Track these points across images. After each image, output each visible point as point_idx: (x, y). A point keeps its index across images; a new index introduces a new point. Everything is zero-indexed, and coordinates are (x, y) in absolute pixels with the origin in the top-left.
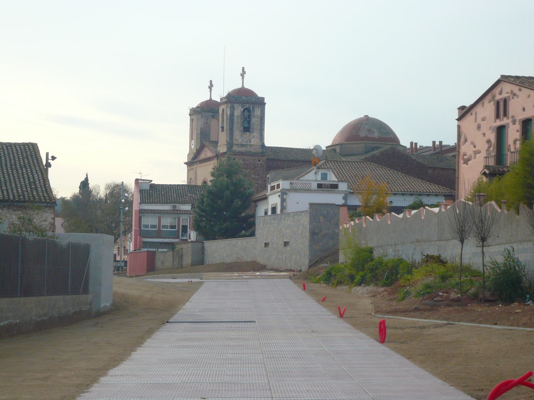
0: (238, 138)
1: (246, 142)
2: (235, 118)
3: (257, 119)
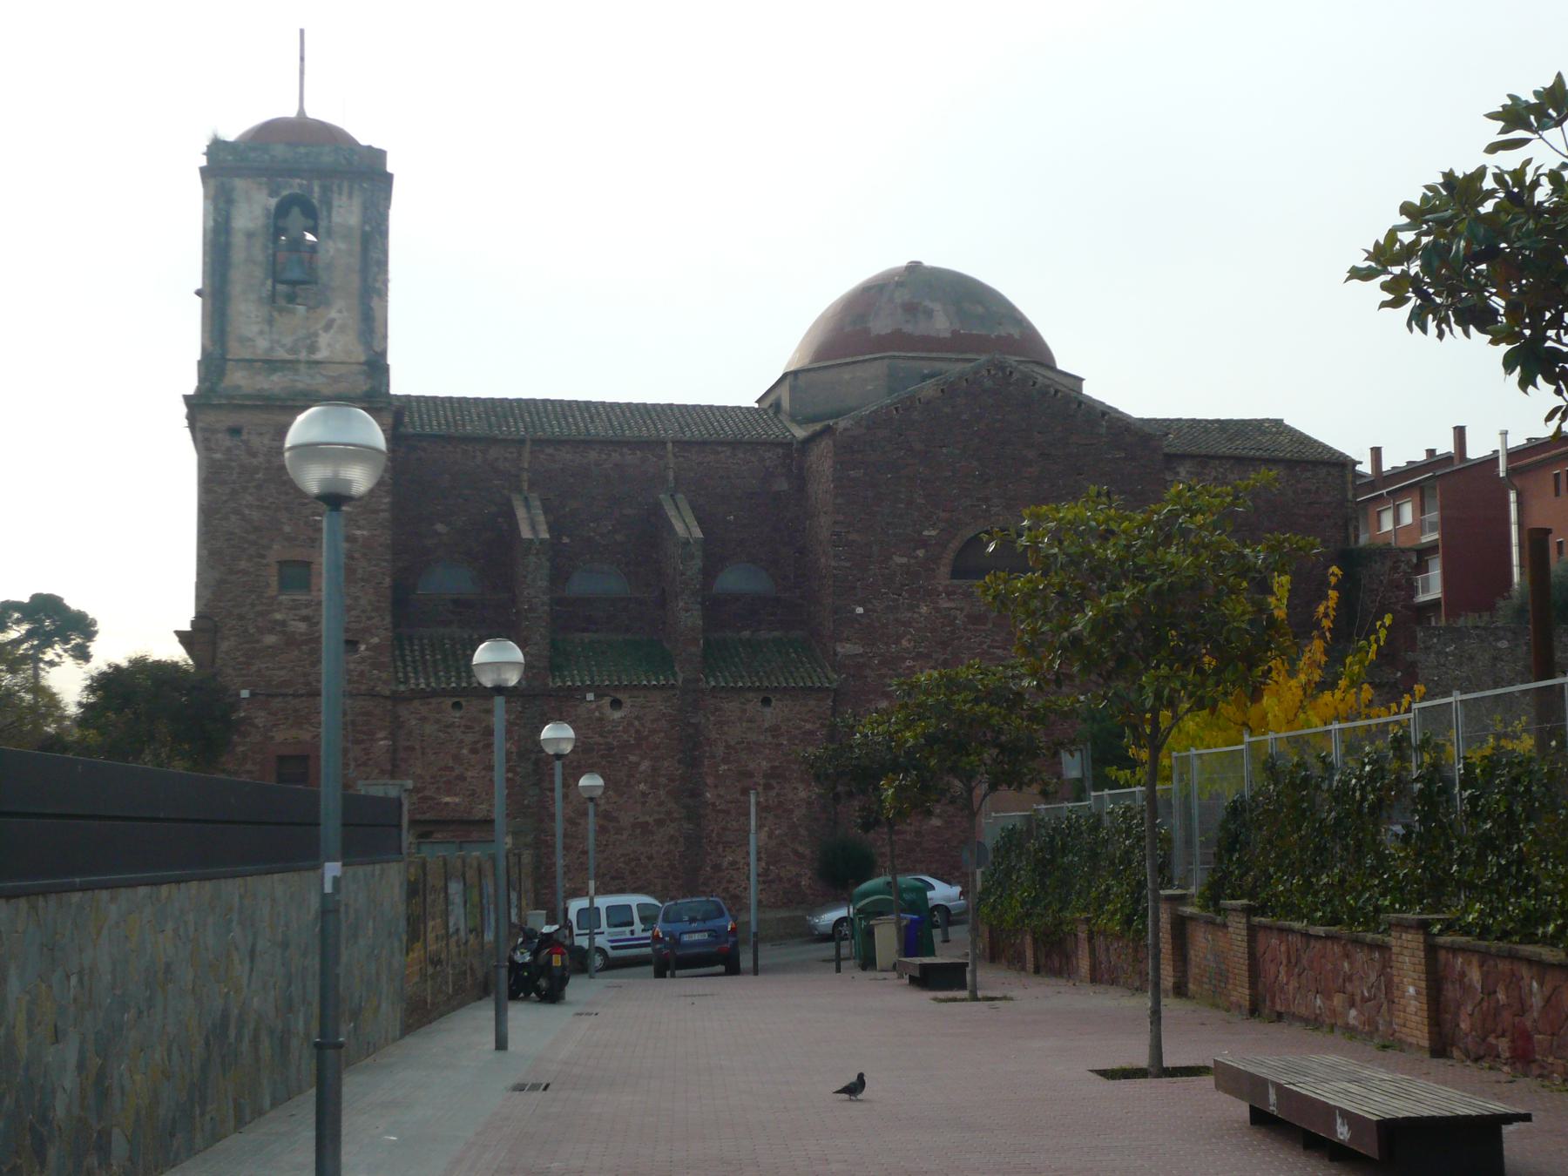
0: (251, 330)
1: (293, 350)
2: (238, 240)
3: (342, 246)
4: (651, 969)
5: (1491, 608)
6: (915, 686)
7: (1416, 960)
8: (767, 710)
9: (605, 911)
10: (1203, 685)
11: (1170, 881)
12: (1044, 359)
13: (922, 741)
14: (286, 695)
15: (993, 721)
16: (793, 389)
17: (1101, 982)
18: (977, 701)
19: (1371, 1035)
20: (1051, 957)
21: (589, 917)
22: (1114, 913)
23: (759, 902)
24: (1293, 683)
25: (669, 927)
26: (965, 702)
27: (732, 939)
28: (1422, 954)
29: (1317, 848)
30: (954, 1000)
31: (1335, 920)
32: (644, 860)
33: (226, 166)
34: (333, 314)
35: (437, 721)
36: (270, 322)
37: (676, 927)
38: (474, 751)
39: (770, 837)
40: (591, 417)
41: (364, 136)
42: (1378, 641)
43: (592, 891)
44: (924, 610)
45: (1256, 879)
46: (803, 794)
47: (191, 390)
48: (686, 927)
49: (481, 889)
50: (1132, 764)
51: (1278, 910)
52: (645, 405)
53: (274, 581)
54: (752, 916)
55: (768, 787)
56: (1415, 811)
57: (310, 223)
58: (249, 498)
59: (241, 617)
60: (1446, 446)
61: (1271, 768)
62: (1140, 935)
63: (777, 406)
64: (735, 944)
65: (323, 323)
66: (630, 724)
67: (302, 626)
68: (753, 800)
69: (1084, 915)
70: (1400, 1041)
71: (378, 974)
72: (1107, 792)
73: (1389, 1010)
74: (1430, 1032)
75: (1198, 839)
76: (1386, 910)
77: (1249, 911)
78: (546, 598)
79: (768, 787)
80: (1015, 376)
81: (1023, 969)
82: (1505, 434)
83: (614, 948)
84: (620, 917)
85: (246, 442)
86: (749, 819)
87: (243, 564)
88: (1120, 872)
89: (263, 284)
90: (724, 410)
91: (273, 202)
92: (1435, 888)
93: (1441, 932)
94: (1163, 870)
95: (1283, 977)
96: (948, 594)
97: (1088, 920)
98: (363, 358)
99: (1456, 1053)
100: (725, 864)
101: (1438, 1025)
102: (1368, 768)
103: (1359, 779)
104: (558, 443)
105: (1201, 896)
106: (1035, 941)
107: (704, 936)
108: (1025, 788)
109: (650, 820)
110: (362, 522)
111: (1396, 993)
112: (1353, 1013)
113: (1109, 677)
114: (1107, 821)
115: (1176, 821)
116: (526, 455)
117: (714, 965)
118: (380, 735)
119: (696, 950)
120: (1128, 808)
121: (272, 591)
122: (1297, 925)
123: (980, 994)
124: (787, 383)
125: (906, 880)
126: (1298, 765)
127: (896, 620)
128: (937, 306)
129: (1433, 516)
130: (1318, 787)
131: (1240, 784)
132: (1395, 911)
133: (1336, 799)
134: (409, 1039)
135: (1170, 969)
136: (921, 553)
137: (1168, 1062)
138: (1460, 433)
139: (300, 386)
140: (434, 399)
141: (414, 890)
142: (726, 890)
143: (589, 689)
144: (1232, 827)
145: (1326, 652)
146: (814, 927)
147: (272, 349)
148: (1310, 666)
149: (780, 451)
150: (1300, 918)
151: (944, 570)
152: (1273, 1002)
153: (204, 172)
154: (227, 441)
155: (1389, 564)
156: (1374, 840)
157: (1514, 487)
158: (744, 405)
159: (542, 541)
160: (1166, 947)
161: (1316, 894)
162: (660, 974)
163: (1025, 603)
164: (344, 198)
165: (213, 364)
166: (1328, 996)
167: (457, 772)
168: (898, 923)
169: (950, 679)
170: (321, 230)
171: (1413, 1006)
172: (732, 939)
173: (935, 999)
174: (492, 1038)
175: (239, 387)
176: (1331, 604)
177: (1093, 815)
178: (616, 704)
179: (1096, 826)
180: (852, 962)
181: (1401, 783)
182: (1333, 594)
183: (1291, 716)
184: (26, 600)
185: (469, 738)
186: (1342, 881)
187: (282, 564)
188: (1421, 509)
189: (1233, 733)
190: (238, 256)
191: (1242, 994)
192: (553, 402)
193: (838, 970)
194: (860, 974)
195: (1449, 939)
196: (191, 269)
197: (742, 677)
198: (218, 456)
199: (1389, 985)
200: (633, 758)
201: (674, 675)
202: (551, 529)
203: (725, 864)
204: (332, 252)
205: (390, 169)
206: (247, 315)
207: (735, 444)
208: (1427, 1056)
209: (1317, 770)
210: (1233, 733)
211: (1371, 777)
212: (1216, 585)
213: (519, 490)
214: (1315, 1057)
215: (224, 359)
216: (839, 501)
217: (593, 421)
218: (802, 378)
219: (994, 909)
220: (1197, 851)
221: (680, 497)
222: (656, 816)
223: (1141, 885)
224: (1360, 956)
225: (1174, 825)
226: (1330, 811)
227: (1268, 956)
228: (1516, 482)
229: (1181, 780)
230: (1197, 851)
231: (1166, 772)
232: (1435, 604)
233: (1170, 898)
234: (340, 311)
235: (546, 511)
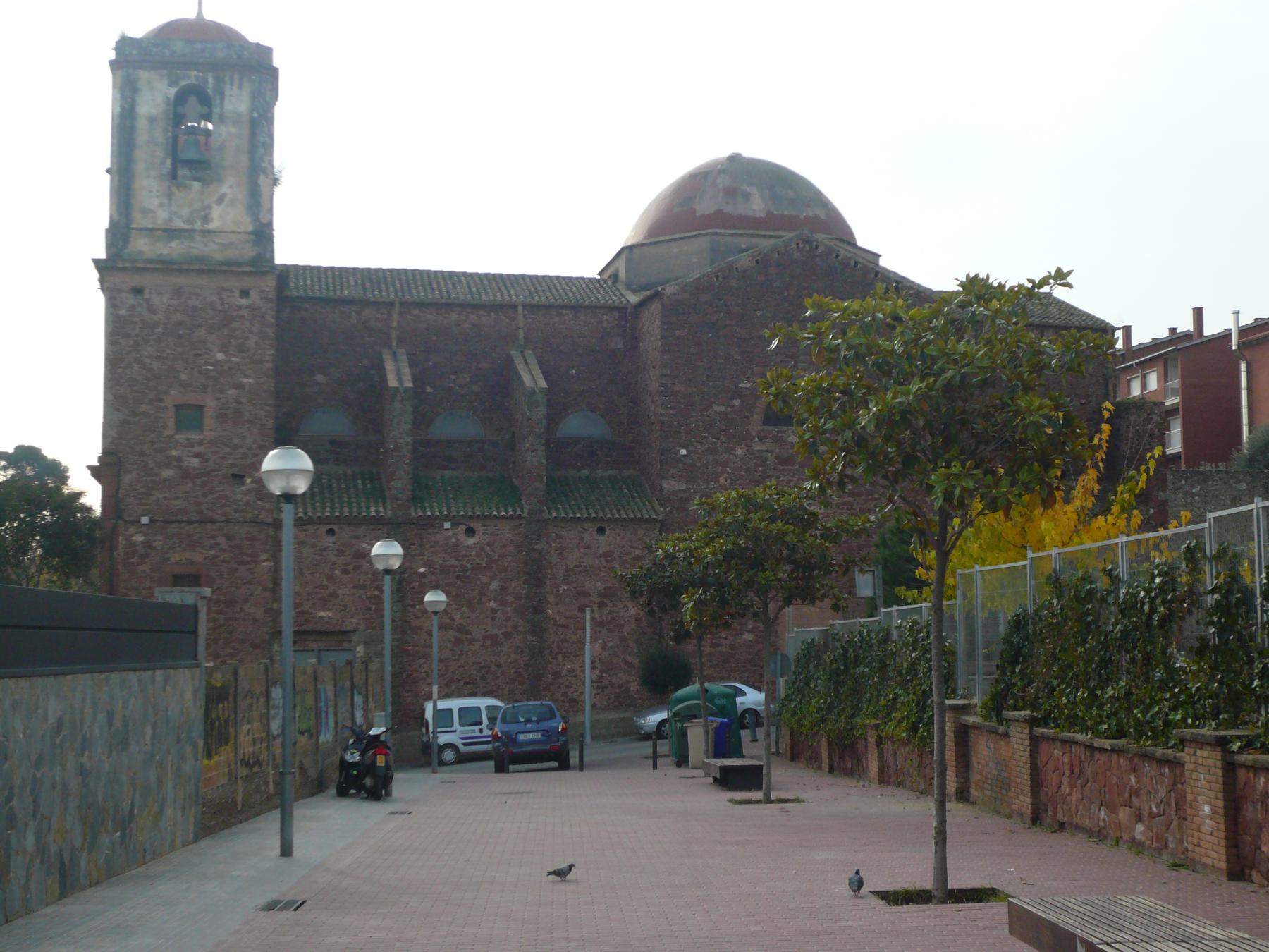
1: (189, 221)
2: (142, 124)
3: (233, 130)
4: (492, 763)
5: (1226, 458)
6: (714, 508)
7: (1213, 778)
8: (602, 539)
9: (456, 714)
10: (997, 485)
11: (954, 691)
12: (846, 237)
13: (720, 557)
14: (180, 522)
15: (788, 539)
16: (628, 261)
17: (888, 783)
18: (773, 520)
19: (1159, 851)
20: (844, 758)
21: (444, 717)
22: (901, 720)
23: (594, 706)
24: (1069, 508)
25: (507, 728)
26: (761, 520)
27: (562, 738)
28: (1220, 772)
29: (1101, 660)
30: (749, 802)
31: (1121, 734)
32: (493, 668)
33: (132, 59)
34: (225, 189)
35: (313, 546)
36: (170, 196)
37: (513, 728)
38: (345, 572)
39: (603, 648)
40: (454, 285)
41: (253, 34)
42: (1147, 471)
43: (435, 696)
44: (739, 452)
45: (1038, 689)
46: (632, 612)
47: (102, 254)
48: (521, 727)
49: (317, 692)
50: (920, 584)
51: (1061, 722)
52: (501, 275)
53: (171, 422)
54: (587, 717)
55: (602, 605)
56: (1211, 623)
57: (206, 110)
58: (149, 349)
59: (142, 454)
60: (1185, 325)
61: (1055, 582)
62: (925, 741)
63: (615, 277)
64: (566, 743)
65: (215, 198)
66: (482, 549)
67: (196, 462)
68: (588, 616)
69: (873, 722)
70: (1193, 860)
71: (160, 781)
72: (895, 608)
73: (1180, 826)
74: (1227, 854)
75: (981, 651)
76: (1176, 725)
77: (1032, 722)
78: (409, 439)
79: (602, 605)
80: (821, 249)
81: (820, 768)
82: (1237, 313)
83: (464, 744)
84: (469, 716)
85: (147, 301)
86: (584, 633)
87: (144, 408)
88: (907, 682)
89: (163, 163)
90: (570, 279)
91: (172, 91)
92: (1234, 704)
93: (1240, 750)
94: (948, 678)
95: (1065, 788)
96: (761, 439)
97: (877, 726)
98: (250, 228)
99: (1255, 876)
100: (564, 672)
101: (1236, 846)
102: (1158, 580)
103: (1148, 591)
104: (421, 305)
105: (985, 706)
106: (830, 744)
107: (538, 736)
108: (818, 603)
109: (499, 633)
110: (248, 372)
111: (1189, 811)
112: (1140, 827)
113: (894, 480)
114: (895, 633)
115: (961, 635)
116: (395, 316)
117: (548, 760)
118: (264, 557)
119: (529, 748)
120: (915, 623)
121: (170, 430)
122: (1081, 737)
123: (774, 795)
124: (623, 257)
125: (717, 687)
126: (1083, 579)
127: (715, 460)
128: (754, 191)
129: (1175, 383)
130: (1103, 600)
131: (1028, 597)
132: (1187, 726)
133: (1122, 612)
134: (205, 843)
135: (954, 778)
136: (737, 402)
137: (954, 883)
138: (1198, 313)
139: (195, 252)
140: (318, 268)
141: (215, 697)
142: (565, 694)
143: (446, 518)
144: (1015, 640)
145: (1099, 481)
146: (641, 727)
147: (170, 220)
148: (1084, 493)
149: (616, 314)
150: (1085, 730)
151: (757, 417)
152: (1055, 813)
153: (114, 65)
154: (130, 300)
155: (1144, 416)
156: (1164, 653)
157: (1245, 359)
158: (587, 275)
159: (407, 389)
160: (950, 755)
161: (1101, 707)
162: (501, 768)
163: (808, 401)
164: (235, 88)
165: (118, 233)
166: (1112, 809)
167: (330, 590)
168: (705, 726)
169: (748, 500)
170: (215, 116)
171: (1208, 825)
172: (562, 738)
173: (731, 801)
174: (276, 842)
175: (141, 252)
176: (1105, 436)
177: (882, 629)
178: (470, 532)
179: (886, 639)
180: (668, 760)
181: (1193, 595)
182: (1106, 428)
183: (1066, 540)
184: (11, 451)
185: (341, 560)
186: (1128, 694)
187: (178, 407)
188: (1165, 377)
189: (1012, 554)
190: (142, 137)
191: (1024, 802)
192: (421, 272)
193: (655, 767)
194: (675, 772)
195: (1251, 757)
196: (104, 156)
197: (580, 509)
198: (122, 312)
199: (1181, 803)
200: (484, 579)
201: (521, 507)
202: (414, 381)
203: (564, 672)
204: (224, 136)
205: (275, 64)
206: (149, 191)
207: (577, 308)
208: (1224, 879)
209: (1103, 583)
210: (1012, 554)
211: (1162, 589)
212: (1010, 380)
213: (390, 347)
214: (1125, 900)
215: (128, 226)
216: (666, 357)
217: (454, 287)
218: (636, 251)
219: (794, 713)
220: (980, 662)
221: (529, 353)
222: (504, 630)
223: (927, 695)
224: (1149, 770)
225: (958, 639)
226: (1117, 623)
227: (1050, 767)
228: (1246, 353)
229: (965, 597)
230: (980, 662)
231: (949, 593)
232: (1176, 457)
233: (955, 708)
234: (231, 187)
235: (412, 364)
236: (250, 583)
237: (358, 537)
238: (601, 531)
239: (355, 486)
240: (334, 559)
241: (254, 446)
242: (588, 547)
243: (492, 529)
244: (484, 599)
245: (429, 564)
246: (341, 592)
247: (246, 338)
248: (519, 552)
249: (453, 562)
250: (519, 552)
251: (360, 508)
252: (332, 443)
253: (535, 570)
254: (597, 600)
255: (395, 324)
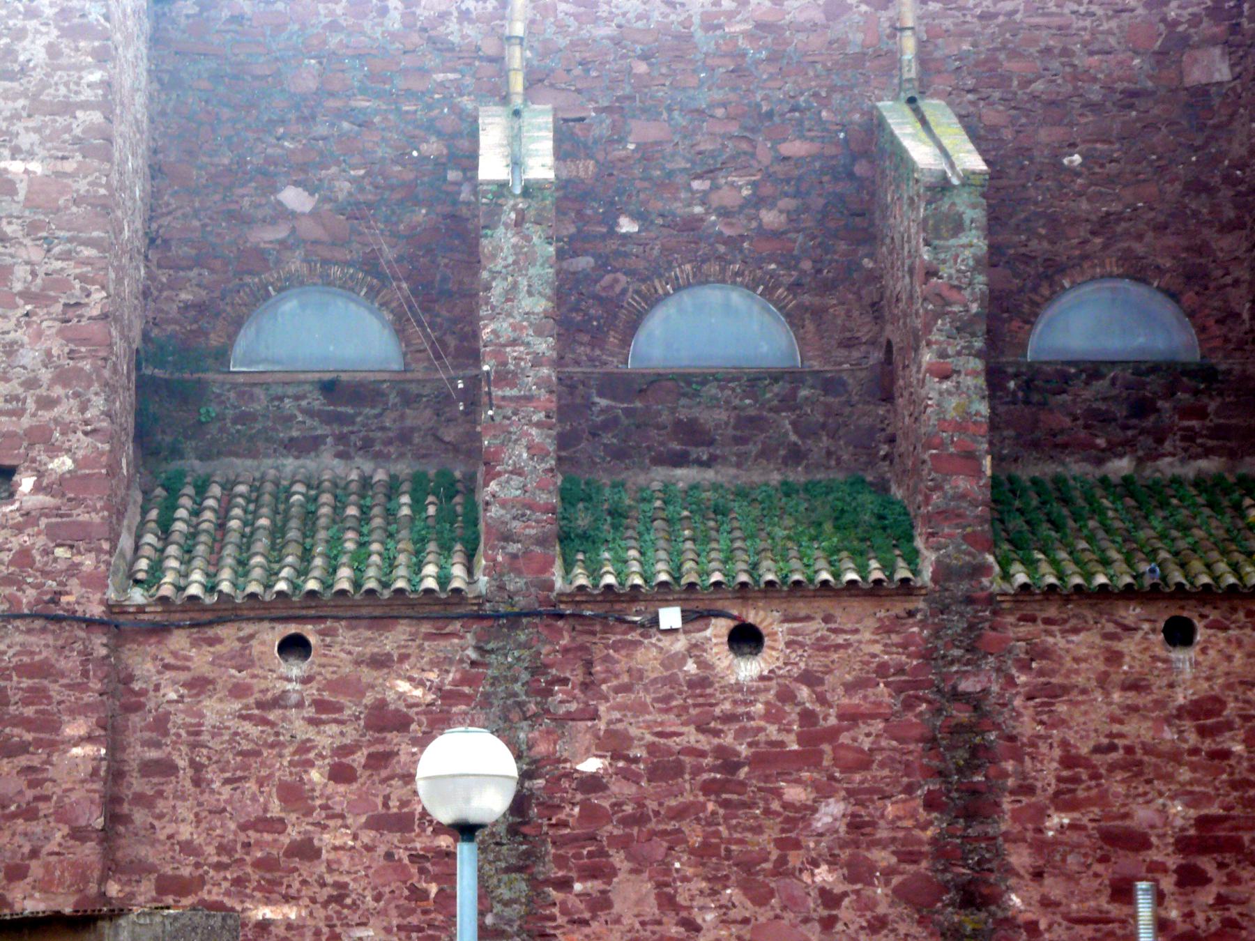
8: (1182, 657)
35: (239, 691)
38: (341, 774)
55: (1190, 878)
66: (786, 696)
68: (1145, 908)
110: (25, 140)
118: (75, 728)
167: (293, 833)
178: (746, 639)
185: (327, 738)
197: (1106, 562)
200: (795, 794)
201: (912, 558)
213: (505, 100)
221: (934, 108)
236: (30, 814)
237: (380, 662)
238: (1179, 634)
239: (390, 514)
240: (302, 730)
241: (45, 375)
242: (1135, 686)
243: (816, 627)
244: (795, 859)
245: (614, 745)
246: (326, 840)
247: (20, 34)
248: (908, 705)
249: (692, 737)
250: (908, 705)
251: (391, 564)
252: (330, 388)
253: (962, 764)
254: (1173, 862)
255: (519, 29)
